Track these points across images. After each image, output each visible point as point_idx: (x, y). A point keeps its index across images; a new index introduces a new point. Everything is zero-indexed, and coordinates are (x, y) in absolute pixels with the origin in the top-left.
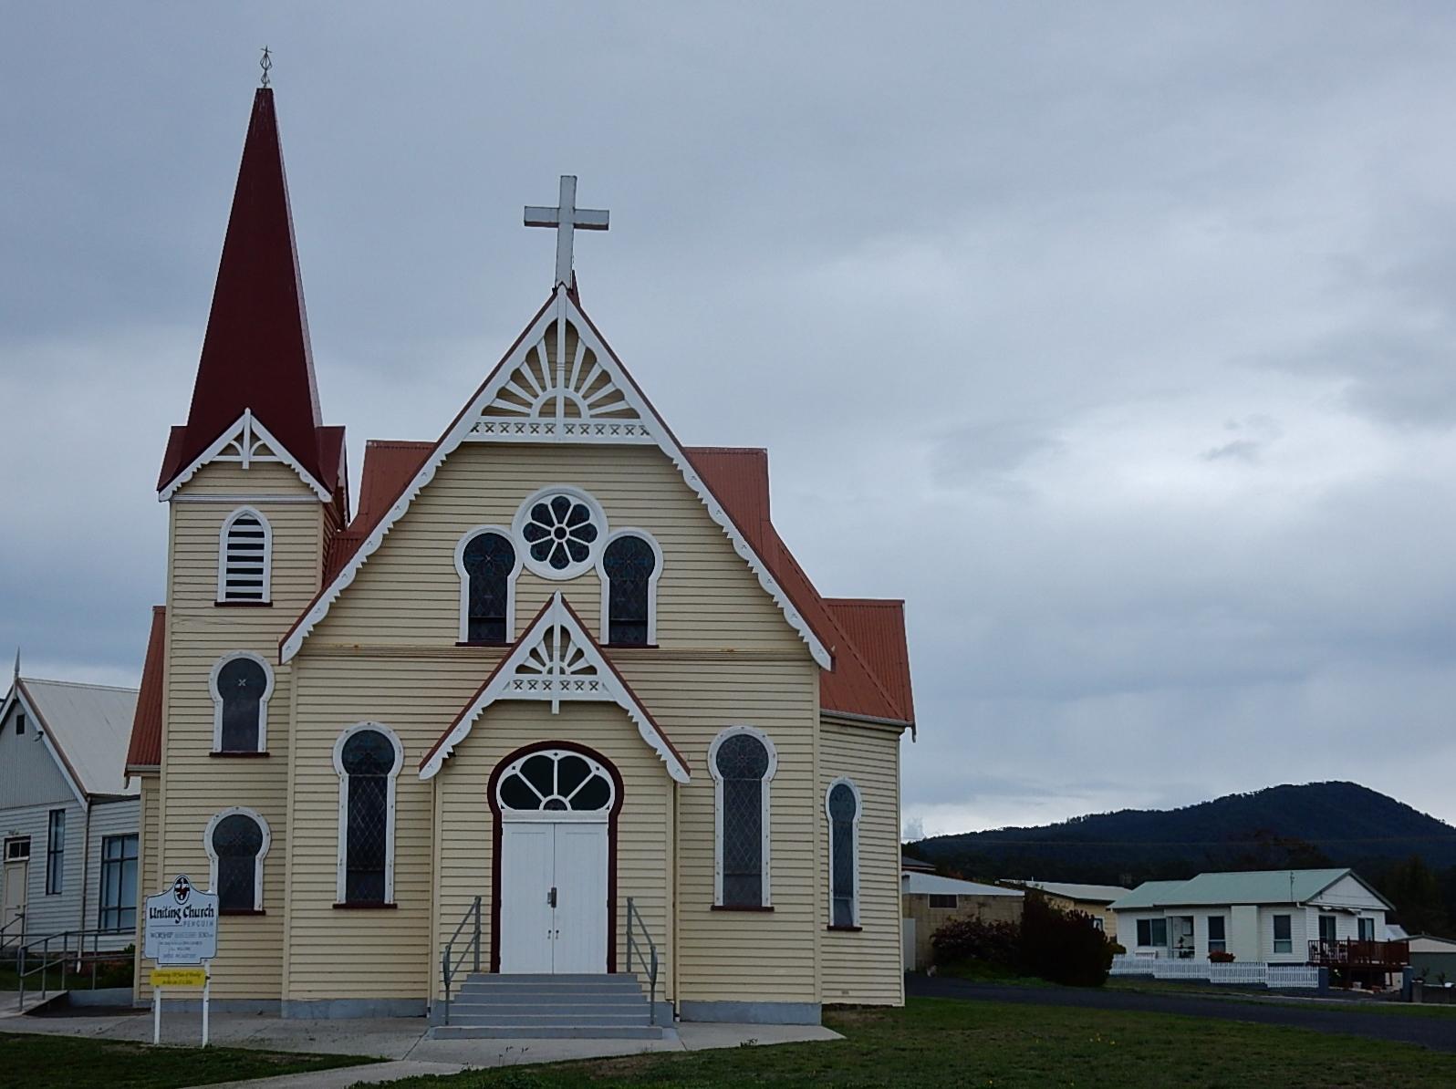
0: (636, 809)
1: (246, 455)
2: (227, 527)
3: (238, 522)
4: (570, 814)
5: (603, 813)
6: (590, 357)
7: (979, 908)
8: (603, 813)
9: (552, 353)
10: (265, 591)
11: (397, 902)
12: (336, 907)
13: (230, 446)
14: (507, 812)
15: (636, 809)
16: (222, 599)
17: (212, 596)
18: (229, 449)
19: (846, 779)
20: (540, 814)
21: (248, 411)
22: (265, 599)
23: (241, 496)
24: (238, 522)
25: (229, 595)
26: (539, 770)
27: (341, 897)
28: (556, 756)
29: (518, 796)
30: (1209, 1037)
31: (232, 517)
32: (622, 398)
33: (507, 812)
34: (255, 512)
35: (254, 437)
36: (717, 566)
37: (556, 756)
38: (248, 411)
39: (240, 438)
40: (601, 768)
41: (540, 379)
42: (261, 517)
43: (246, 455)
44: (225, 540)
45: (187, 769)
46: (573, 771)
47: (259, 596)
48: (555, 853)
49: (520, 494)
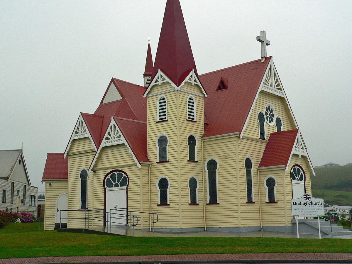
0: (132, 183)
1: (159, 83)
2: (158, 101)
3: (161, 100)
4: (120, 188)
5: (125, 187)
6: (277, 81)
7: (87, 209)
8: (125, 187)
9: (268, 78)
10: (195, 118)
11: (170, 203)
13: (157, 80)
15: (132, 183)
16: (158, 121)
17: (155, 120)
18: (157, 81)
19: (250, 157)
20: (114, 188)
21: (159, 70)
22: (195, 120)
23: (189, 91)
24: (161, 100)
26: (113, 177)
27: (159, 203)
28: (116, 173)
29: (110, 185)
31: (159, 99)
33: (107, 188)
34: (193, 97)
35: (161, 76)
36: (285, 118)
40: (125, 175)
41: (267, 82)
42: (194, 99)
43: (160, 82)
45: (136, 176)
46: (120, 175)
47: (194, 119)
48: (116, 197)
49: (266, 103)
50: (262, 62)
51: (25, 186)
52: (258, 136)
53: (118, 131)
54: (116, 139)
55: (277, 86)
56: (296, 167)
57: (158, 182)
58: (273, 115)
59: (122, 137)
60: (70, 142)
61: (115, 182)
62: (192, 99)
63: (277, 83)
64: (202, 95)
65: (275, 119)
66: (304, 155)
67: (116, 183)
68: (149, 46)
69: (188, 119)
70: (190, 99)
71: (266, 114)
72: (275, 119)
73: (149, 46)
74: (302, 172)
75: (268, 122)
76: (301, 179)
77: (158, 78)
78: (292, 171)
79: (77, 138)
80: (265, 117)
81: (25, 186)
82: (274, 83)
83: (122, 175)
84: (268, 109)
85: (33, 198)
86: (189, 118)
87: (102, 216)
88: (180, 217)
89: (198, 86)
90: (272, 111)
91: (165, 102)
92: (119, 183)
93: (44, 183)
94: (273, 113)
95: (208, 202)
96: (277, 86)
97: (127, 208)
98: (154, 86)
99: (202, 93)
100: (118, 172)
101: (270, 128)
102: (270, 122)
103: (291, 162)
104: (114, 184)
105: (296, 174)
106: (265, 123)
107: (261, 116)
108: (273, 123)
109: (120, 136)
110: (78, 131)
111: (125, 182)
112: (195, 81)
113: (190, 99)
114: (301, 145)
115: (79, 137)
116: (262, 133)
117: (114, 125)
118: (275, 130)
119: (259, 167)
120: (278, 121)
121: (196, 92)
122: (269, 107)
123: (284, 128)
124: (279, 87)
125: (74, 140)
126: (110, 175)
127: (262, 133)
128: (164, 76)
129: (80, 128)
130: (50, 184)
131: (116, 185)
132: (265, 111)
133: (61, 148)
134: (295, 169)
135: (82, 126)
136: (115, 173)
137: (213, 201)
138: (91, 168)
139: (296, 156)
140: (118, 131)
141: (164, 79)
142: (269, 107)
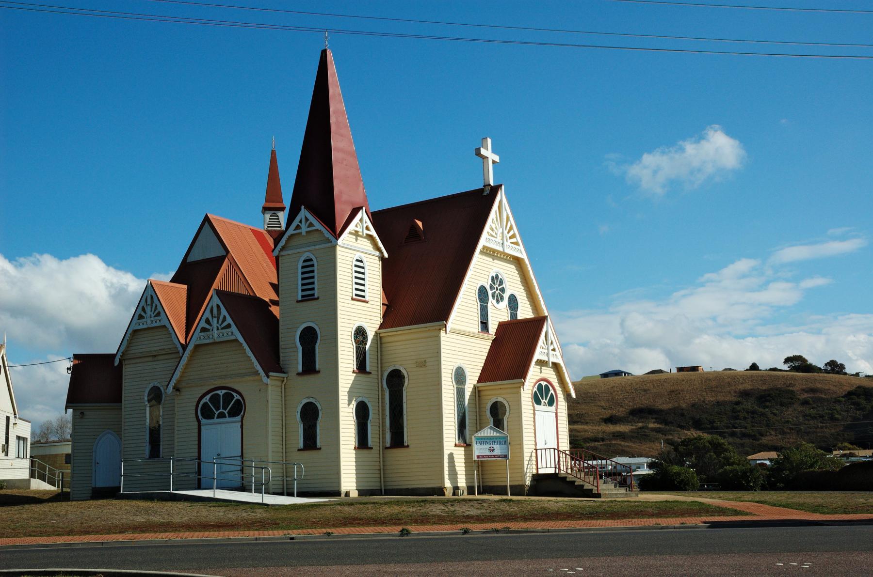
2: (301, 264)
4: (228, 419)
5: (239, 418)
12: (299, 450)
14: (204, 421)
16: (300, 298)
18: (298, 227)
20: (216, 420)
21: (303, 207)
24: (305, 261)
25: (303, 296)
27: (301, 445)
28: (221, 393)
29: (207, 413)
30: (612, 428)
32: (313, 226)
33: (204, 421)
35: (307, 220)
37: (221, 393)
38: (303, 207)
39: (300, 222)
42: (364, 260)
44: (300, 270)
46: (228, 398)
47: (364, 297)
50: (485, 194)
51: (8, 418)
52: (476, 327)
53: (225, 317)
54: (153, 319)
55: (511, 238)
56: (541, 382)
57: (299, 409)
58: (503, 290)
59: (234, 328)
60: (128, 335)
61: (218, 408)
62: (361, 261)
63: (511, 233)
64: (377, 253)
65: (506, 297)
66: (555, 361)
67: (221, 410)
68: (273, 152)
69: (354, 297)
70: (357, 260)
71: (492, 288)
72: (506, 297)
73: (273, 152)
74: (552, 391)
75: (494, 302)
76: (551, 403)
77: (300, 222)
78: (535, 389)
79: (141, 327)
80: (490, 293)
81: (8, 418)
82: (506, 232)
83: (233, 397)
84: (496, 279)
85: (21, 442)
86: (356, 295)
87: (193, 470)
88: (538, 355)
89: (370, 237)
90: (501, 283)
91: (313, 266)
92: (226, 412)
93: (70, 411)
94: (504, 286)
95: (388, 445)
96: (511, 238)
97: (242, 456)
98: (292, 236)
99: (379, 249)
100: (224, 391)
101: (499, 314)
102: (498, 301)
103: (534, 374)
104: (217, 413)
105: (542, 394)
106: (489, 305)
107: (482, 293)
108: (505, 303)
109: (229, 326)
110: (143, 314)
111: (238, 409)
112: (367, 228)
113: (357, 260)
114: (552, 343)
115: (145, 326)
116: (484, 325)
117: (218, 306)
118: (505, 317)
119: (478, 382)
120: (513, 302)
121: (367, 245)
122: (497, 276)
123: (525, 312)
124: (514, 240)
125: (135, 332)
126: (208, 397)
127: (484, 325)
128: (312, 219)
129: (148, 309)
130: (82, 413)
131: (222, 415)
132: (490, 282)
133: (110, 345)
134: (540, 386)
135: (152, 304)
136: (219, 392)
137: (398, 441)
138: (172, 384)
139: (541, 363)
140: (225, 317)
141: (311, 225)
142: (497, 276)
